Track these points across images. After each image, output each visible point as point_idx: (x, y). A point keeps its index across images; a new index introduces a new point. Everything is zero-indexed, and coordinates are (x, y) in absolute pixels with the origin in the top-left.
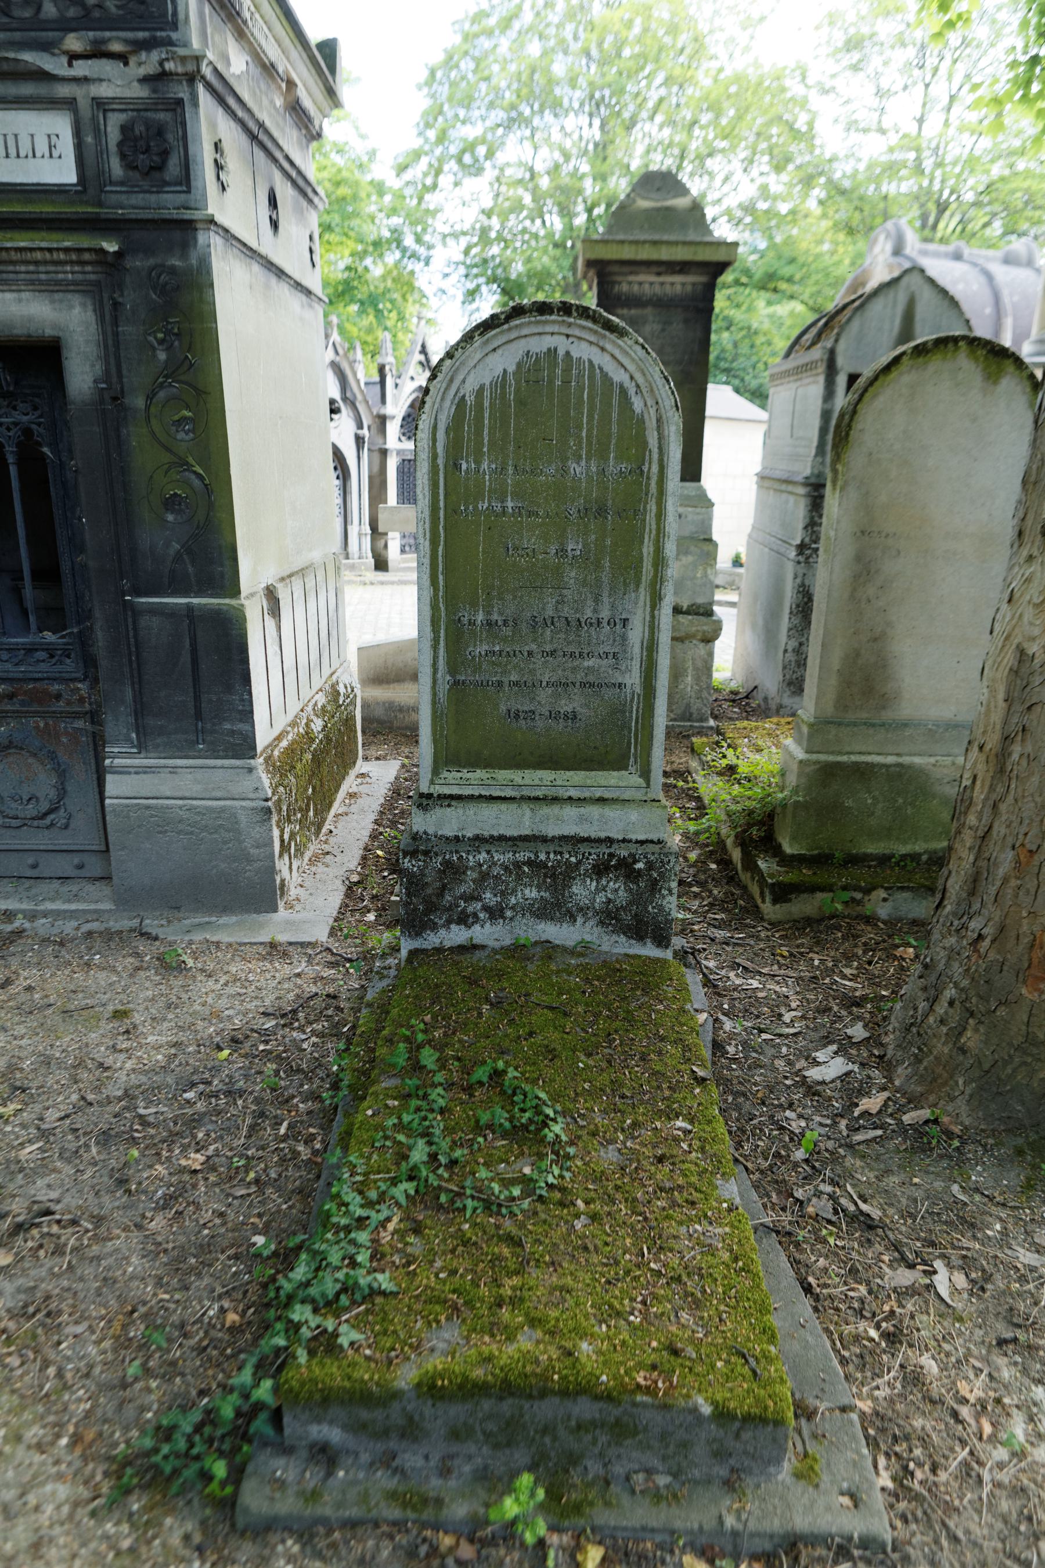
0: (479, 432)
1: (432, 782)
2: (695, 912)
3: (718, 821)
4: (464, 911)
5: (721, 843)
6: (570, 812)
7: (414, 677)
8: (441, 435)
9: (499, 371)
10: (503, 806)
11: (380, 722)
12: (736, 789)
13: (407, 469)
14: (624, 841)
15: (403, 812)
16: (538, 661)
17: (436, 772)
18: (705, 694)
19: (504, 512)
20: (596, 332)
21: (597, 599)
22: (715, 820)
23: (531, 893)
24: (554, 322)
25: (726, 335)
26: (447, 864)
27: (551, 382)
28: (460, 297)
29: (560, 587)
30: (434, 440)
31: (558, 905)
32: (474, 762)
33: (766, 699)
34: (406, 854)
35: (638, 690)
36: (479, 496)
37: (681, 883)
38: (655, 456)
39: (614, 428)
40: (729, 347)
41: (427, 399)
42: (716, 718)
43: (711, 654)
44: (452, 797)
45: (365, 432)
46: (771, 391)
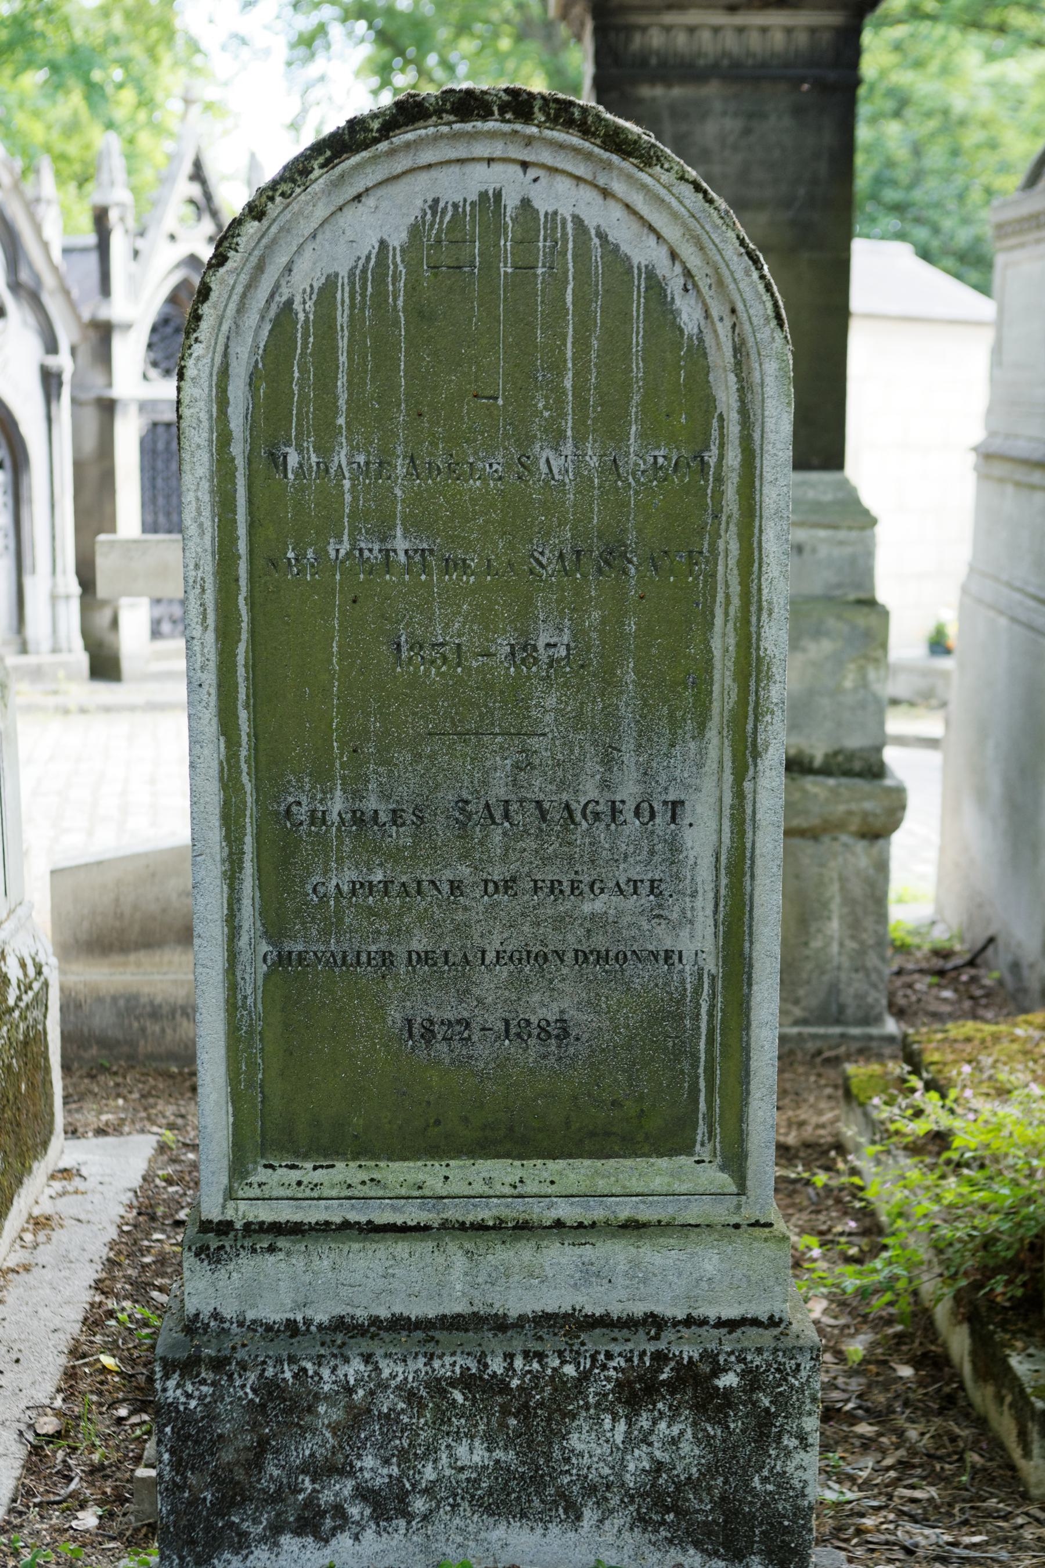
0: (325, 384)
1: (230, 1195)
2: (866, 1485)
3: (911, 1265)
4: (311, 1502)
5: (922, 1316)
6: (559, 1256)
7: (185, 936)
8: (238, 391)
9: (369, 244)
10: (401, 1248)
11: (104, 1043)
12: (952, 1189)
13: (163, 445)
14: (689, 1321)
15: (162, 1260)
16: (476, 902)
17: (238, 1170)
18: (872, 960)
19: (388, 564)
20: (588, 156)
21: (609, 759)
22: (906, 1261)
23: (473, 1454)
24: (492, 135)
25: (893, 128)
26: (270, 1389)
27: (489, 266)
28: (281, 51)
29: (521, 732)
30: (223, 402)
31: (537, 1481)
32: (329, 1144)
33: (1015, 967)
34: (170, 1367)
35: (711, 964)
36: (331, 527)
37: (829, 1414)
38: (733, 430)
39: (637, 368)
40: (901, 153)
41: (206, 309)
42: (900, 1013)
43: (882, 867)
44: (277, 1229)
45: (63, 361)
46: (1000, 260)
